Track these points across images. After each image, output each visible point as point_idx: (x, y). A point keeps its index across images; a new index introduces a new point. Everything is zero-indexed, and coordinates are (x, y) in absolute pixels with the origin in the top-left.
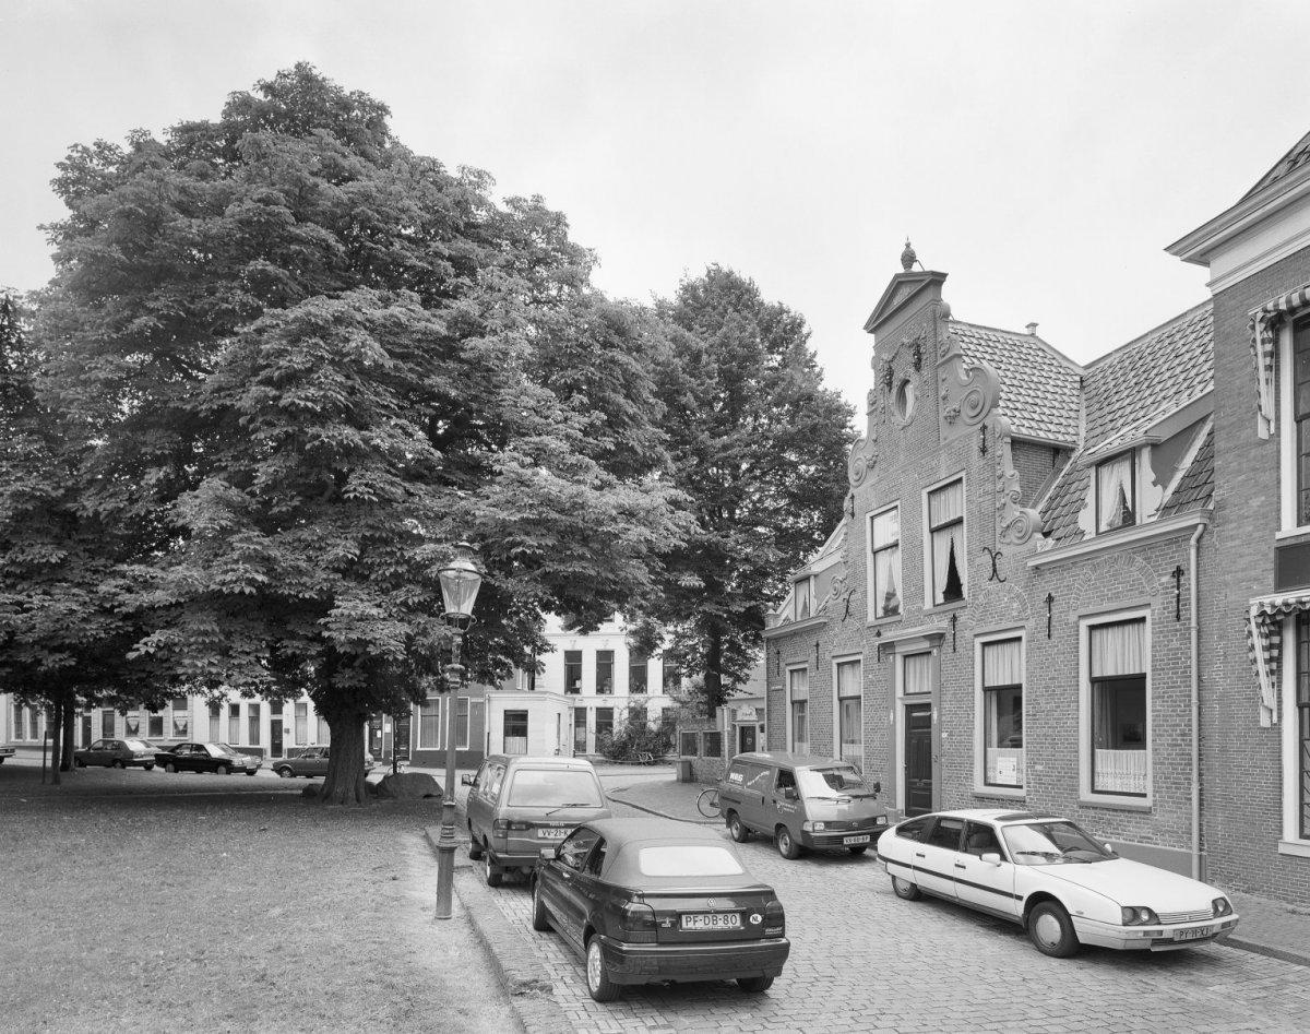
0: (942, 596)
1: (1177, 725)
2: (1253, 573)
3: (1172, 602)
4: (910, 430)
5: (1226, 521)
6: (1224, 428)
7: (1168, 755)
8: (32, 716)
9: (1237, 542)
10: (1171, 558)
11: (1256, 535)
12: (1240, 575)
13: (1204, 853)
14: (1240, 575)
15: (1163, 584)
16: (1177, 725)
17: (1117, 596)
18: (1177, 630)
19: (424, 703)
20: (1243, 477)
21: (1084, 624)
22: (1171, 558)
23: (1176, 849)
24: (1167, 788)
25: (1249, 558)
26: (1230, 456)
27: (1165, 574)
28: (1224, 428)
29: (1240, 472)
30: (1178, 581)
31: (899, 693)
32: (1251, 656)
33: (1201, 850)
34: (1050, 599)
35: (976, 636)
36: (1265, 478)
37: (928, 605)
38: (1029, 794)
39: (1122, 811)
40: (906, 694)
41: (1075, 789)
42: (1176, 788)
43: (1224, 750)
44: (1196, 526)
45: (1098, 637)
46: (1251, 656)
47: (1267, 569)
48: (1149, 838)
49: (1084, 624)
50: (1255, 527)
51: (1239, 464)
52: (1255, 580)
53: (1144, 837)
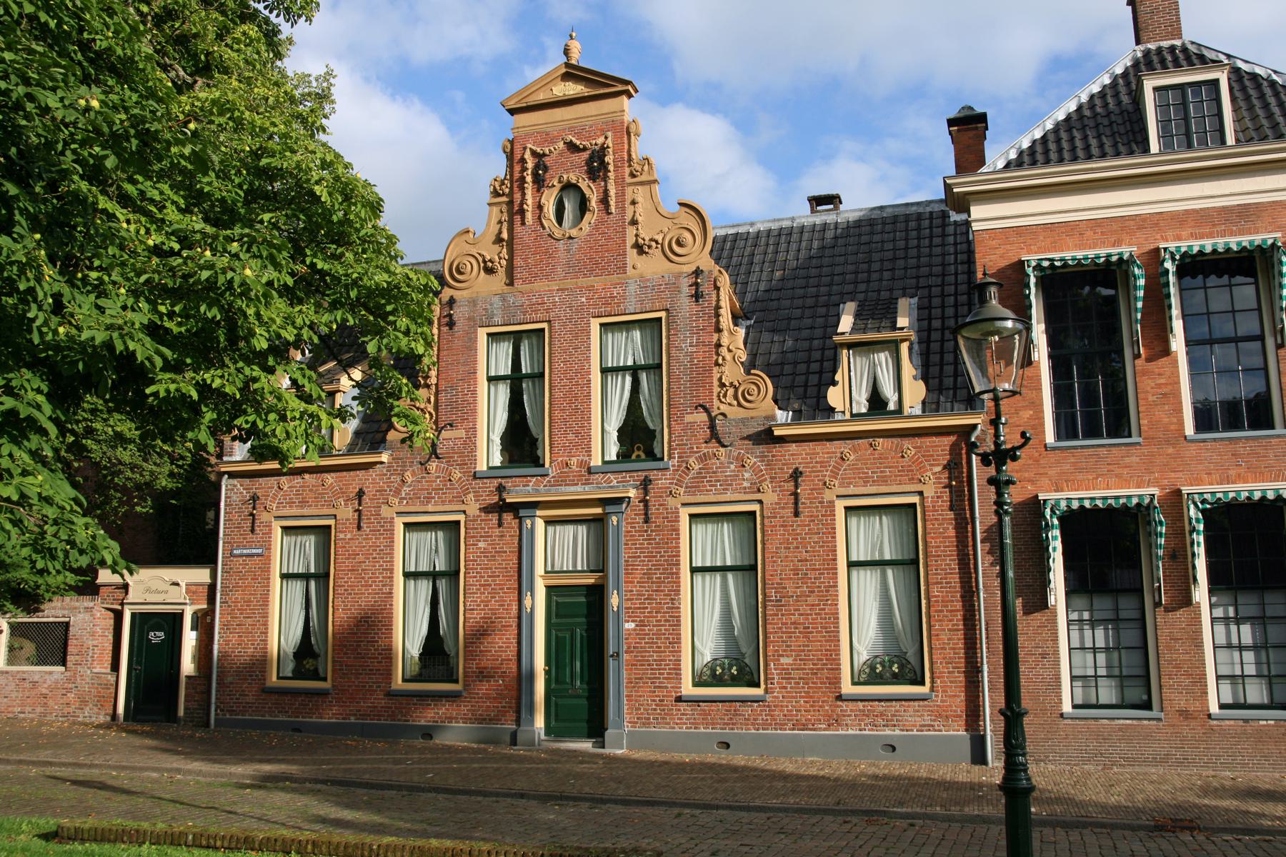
2: (1026, 475)
40: (546, 572)
41: (836, 681)
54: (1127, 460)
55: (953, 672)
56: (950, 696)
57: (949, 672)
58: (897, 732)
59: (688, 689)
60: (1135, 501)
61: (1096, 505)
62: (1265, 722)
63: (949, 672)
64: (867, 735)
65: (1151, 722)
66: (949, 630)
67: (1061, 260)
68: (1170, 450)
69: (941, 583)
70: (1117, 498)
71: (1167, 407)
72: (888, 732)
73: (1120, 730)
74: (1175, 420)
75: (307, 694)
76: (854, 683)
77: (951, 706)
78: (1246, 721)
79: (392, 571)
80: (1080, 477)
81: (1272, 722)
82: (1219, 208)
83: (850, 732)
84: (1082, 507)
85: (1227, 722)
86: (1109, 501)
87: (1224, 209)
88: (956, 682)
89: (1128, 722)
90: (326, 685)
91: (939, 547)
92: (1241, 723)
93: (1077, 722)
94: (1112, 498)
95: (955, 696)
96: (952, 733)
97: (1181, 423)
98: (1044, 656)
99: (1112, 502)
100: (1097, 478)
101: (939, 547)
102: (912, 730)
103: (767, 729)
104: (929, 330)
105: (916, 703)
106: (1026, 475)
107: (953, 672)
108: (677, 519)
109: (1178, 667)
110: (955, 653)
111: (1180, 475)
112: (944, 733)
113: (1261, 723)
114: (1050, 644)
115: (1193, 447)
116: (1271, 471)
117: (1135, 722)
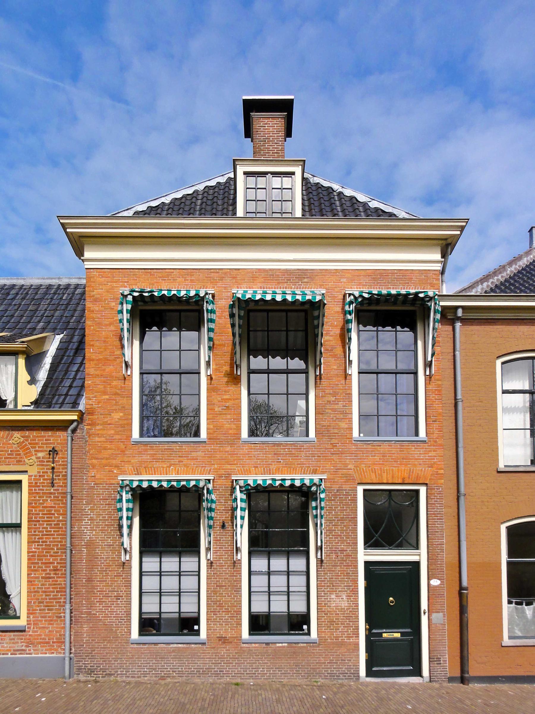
1: (51, 563)
2: (114, 462)
3: (47, 472)
5: (93, 424)
7: (42, 585)
9: (103, 439)
11: (117, 437)
12: (104, 461)
13: (72, 655)
14: (104, 461)
15: (39, 458)
16: (51, 563)
18: (51, 493)
20: (107, 397)
21: (499, 362)
23: (48, 655)
25: (110, 452)
27: (42, 451)
28: (93, 360)
32: (118, 506)
33: (70, 653)
36: (350, 570)
44: (73, 421)
46: (118, 506)
47: (232, 388)
49: (499, 362)
50: (115, 432)
51: (105, 387)
52: (115, 467)
53: (18, 650)
54: (194, 454)
55: (44, 610)
56: (40, 628)
57: (40, 610)
60: (193, 483)
61: (161, 486)
62: (280, 645)
63: (40, 610)
64: (18, 658)
65: (197, 646)
66: (42, 578)
67: (149, 292)
68: (228, 449)
69: (39, 542)
70: (179, 481)
71: (229, 416)
73: (173, 651)
74: (234, 426)
77: (40, 635)
78: (267, 644)
80: (156, 465)
81: (286, 644)
82: (284, 270)
84: (150, 487)
85: (253, 645)
86: (173, 483)
87: (287, 271)
88: (45, 617)
89: (180, 645)
90: (22, 622)
91: (39, 514)
92: (264, 645)
93: (141, 646)
94: (184, 480)
95: (44, 628)
96: (40, 655)
97: (239, 428)
98: (118, 597)
99: (175, 484)
100: (170, 467)
101: (39, 514)
102: (7, 654)
103: (53, 653)
104: (70, 342)
105: (12, 634)
106: (114, 462)
107: (44, 610)
109: (220, 606)
110: (46, 596)
111: (234, 467)
112: (33, 655)
113: (278, 645)
114: (123, 589)
115: (246, 447)
116: (302, 467)
117: (185, 646)
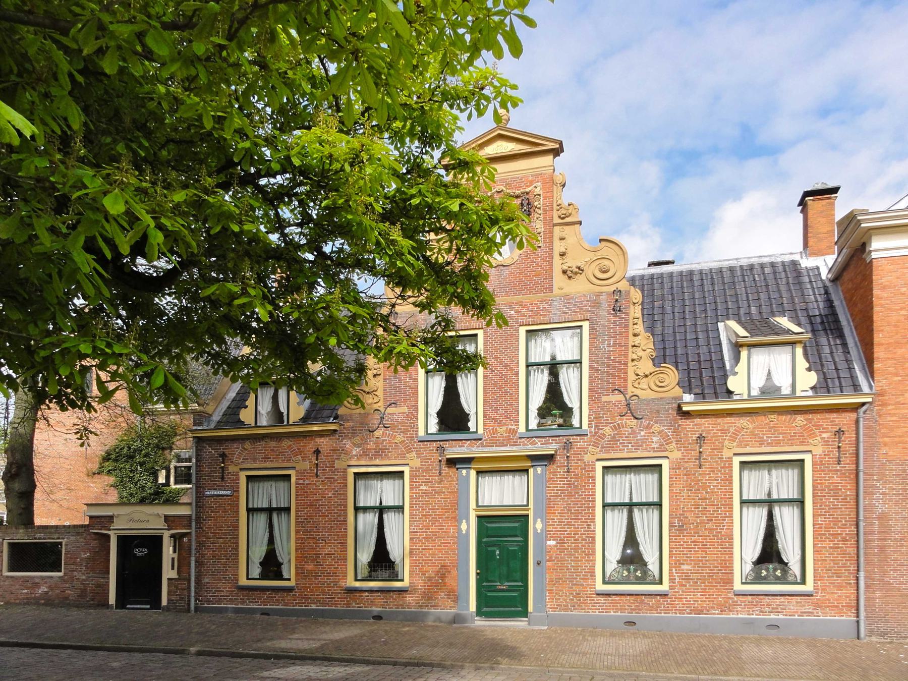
0: (434, 421)
4: (506, 272)
6: (882, 344)
8: (68, 47)
10: (831, 422)
12: (897, 439)
14: (897, 439)
15: (824, 438)
17: (778, 443)
19: (23, 509)
20: (900, 378)
22: (831, 422)
23: (837, 618)
24: (828, 577)
26: (888, 363)
28: (882, 344)
29: (896, 375)
30: (839, 438)
31: (473, 505)
34: (701, 438)
35: (598, 460)
37: (522, 429)
38: (671, 588)
39: (628, 595)
40: (478, 506)
41: (730, 582)
42: (837, 577)
43: (882, 550)
45: (256, 488)
48: (810, 612)
58: (781, 616)
59: (738, 586)
72: (772, 616)
75: (636, 595)
76: (604, 582)
79: (346, 506)
83: (740, 616)
108: (594, 470)
